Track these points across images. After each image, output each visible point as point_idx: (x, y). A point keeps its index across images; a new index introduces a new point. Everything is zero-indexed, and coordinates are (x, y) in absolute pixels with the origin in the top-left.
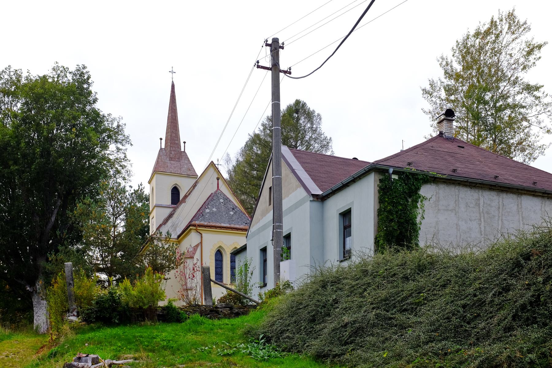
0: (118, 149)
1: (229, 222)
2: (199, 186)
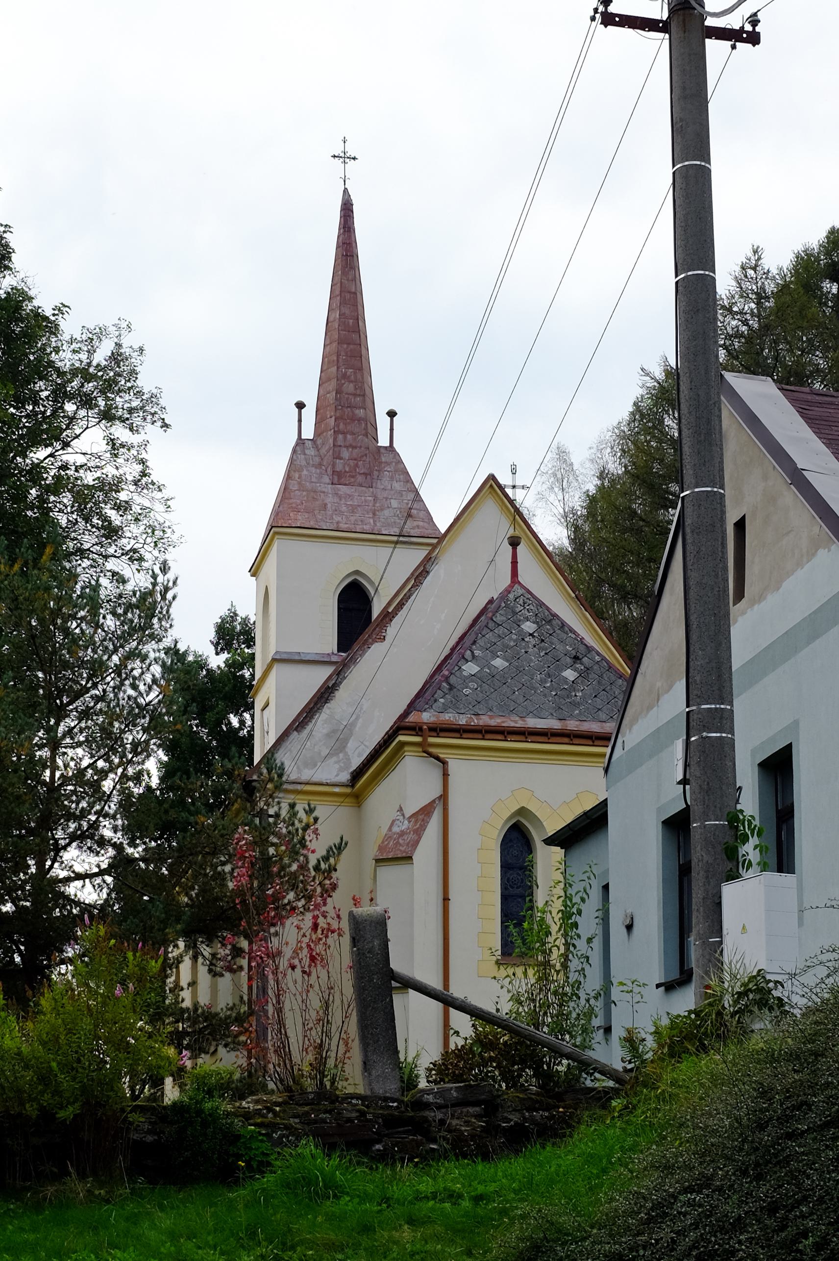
0: (114, 446)
1: (559, 712)
2: (438, 573)
